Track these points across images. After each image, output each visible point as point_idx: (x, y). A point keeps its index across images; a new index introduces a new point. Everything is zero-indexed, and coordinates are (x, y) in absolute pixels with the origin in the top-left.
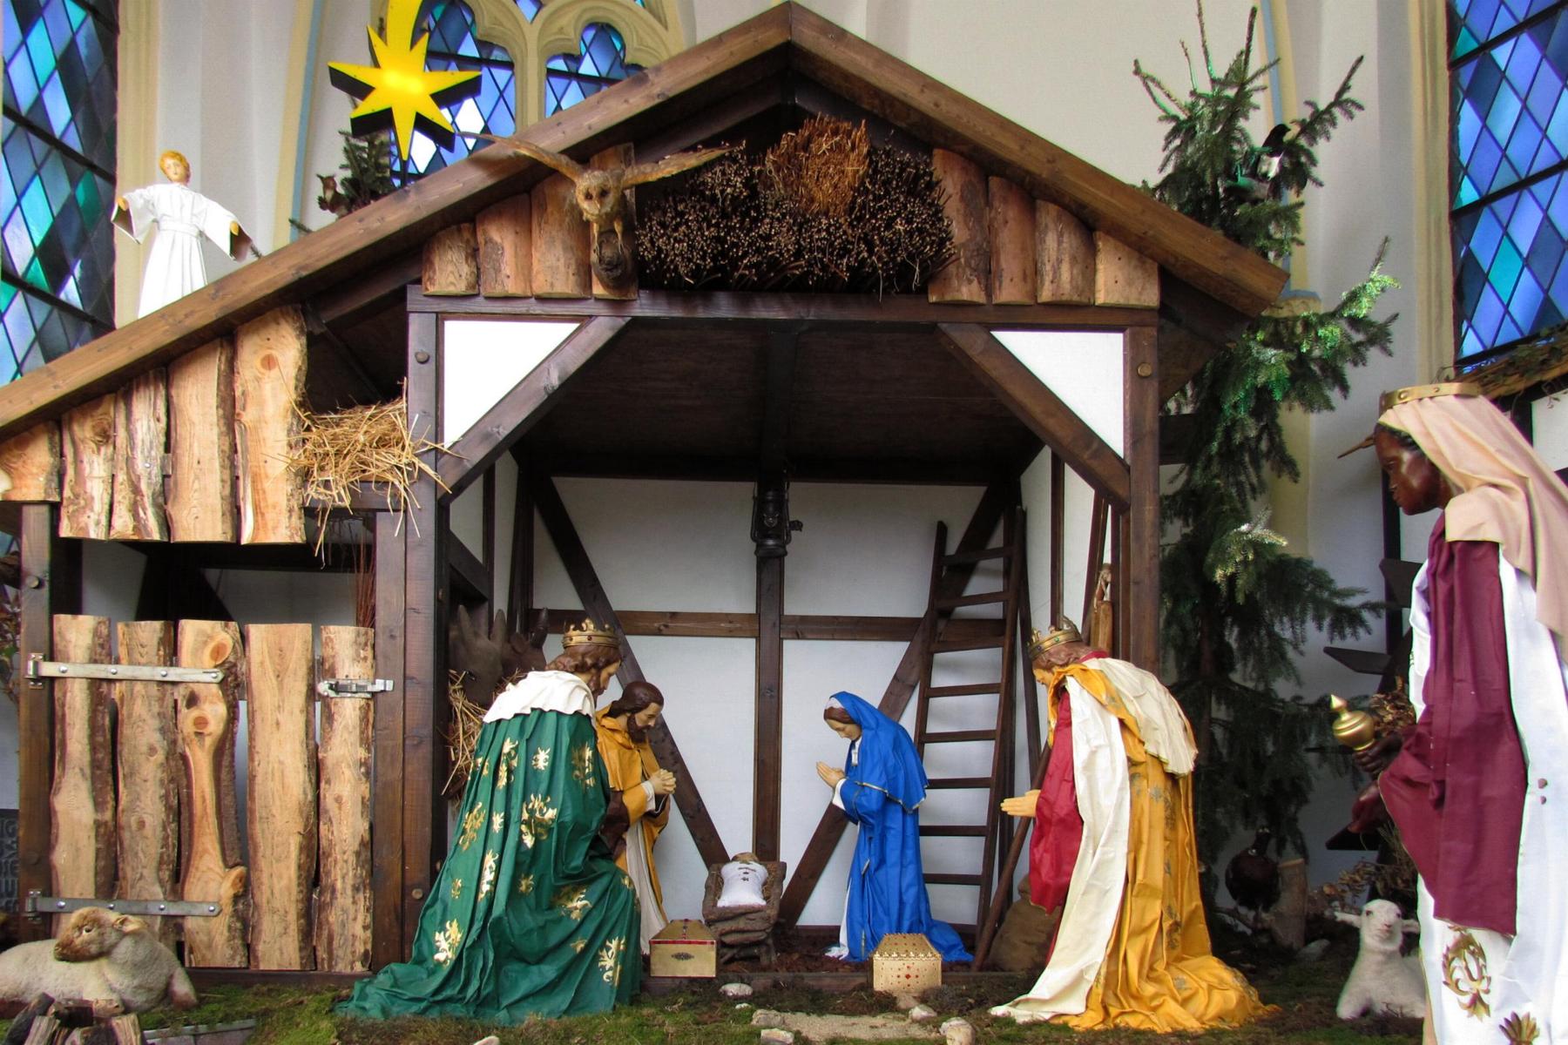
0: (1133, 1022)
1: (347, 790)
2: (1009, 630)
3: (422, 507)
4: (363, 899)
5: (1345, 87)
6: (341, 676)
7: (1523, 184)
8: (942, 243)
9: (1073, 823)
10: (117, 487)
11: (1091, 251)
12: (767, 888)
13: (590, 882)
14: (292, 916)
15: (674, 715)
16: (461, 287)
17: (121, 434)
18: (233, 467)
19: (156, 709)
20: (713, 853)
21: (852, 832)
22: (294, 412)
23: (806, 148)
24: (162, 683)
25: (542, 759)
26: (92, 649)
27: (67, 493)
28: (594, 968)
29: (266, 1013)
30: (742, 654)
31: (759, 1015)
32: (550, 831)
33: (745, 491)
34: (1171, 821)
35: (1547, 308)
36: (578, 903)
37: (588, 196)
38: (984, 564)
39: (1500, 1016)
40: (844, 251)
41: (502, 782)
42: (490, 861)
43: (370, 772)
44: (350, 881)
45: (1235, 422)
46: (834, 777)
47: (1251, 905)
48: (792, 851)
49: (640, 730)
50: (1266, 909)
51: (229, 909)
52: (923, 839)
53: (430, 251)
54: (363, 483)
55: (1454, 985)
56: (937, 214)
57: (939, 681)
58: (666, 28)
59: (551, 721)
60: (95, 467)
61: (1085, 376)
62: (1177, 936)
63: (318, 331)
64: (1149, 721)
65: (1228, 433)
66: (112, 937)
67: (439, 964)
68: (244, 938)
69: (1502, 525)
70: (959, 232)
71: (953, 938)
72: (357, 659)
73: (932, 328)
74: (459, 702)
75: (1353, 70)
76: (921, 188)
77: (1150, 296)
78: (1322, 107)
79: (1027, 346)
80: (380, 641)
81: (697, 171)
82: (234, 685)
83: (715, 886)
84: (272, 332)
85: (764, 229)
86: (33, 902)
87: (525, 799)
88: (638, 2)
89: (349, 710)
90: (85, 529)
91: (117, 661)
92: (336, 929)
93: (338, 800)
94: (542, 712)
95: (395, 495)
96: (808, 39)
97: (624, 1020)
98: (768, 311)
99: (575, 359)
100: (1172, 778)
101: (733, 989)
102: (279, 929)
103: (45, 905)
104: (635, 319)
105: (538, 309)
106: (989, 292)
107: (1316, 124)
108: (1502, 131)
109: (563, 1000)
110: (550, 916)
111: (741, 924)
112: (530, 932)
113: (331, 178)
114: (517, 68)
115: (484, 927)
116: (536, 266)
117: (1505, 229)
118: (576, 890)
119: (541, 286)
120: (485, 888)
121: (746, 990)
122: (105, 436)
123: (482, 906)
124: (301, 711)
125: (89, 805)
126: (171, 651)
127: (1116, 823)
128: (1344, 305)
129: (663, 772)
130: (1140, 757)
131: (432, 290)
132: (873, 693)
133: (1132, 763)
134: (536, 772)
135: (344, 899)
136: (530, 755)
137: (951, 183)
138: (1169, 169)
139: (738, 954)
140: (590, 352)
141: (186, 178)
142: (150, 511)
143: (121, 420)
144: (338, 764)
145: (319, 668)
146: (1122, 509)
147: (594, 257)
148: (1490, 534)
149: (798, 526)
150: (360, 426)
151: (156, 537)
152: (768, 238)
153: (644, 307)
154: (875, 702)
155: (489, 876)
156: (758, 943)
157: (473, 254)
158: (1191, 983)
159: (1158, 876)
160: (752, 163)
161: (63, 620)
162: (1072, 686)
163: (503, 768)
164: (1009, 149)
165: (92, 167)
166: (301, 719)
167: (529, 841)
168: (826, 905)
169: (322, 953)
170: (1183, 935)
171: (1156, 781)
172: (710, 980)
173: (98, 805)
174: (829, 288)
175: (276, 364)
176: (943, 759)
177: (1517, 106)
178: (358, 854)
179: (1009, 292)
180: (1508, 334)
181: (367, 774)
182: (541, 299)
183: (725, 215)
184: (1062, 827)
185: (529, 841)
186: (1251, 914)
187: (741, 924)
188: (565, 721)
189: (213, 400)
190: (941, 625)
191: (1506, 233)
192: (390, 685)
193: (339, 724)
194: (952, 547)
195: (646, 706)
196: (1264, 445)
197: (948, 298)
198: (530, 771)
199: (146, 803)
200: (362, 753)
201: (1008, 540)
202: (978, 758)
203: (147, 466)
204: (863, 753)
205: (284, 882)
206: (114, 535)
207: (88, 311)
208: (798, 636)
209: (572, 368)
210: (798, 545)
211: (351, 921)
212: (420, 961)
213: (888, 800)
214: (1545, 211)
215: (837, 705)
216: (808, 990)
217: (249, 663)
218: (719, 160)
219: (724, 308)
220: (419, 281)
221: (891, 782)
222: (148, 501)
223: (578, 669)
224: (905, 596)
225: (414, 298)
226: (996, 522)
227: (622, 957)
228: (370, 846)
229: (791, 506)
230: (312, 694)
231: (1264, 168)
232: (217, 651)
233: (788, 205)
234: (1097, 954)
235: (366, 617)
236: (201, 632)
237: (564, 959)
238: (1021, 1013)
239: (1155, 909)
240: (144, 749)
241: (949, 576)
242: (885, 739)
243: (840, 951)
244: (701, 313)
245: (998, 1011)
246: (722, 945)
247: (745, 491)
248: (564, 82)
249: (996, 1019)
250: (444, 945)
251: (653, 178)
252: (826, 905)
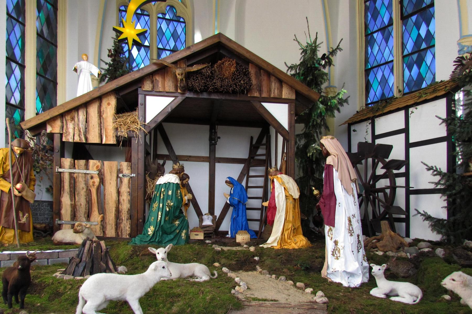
0: (286, 247)
1: (125, 197)
2: (266, 163)
3: (141, 136)
4: (129, 222)
5: (339, 46)
6: (124, 173)
7: (379, 66)
8: (251, 86)
9: (275, 208)
10: (75, 130)
11: (281, 87)
12: (213, 221)
13: (179, 218)
14: (114, 225)
15: (191, 182)
16: (150, 89)
17: (76, 119)
18: (101, 127)
19: (84, 179)
20: (199, 214)
21: (231, 209)
22: (114, 116)
23: (223, 64)
24: (85, 174)
25: (170, 193)
26: (70, 166)
27: (64, 131)
28: (180, 236)
29: (113, 245)
30: (206, 166)
31: (214, 246)
32: (172, 207)
33: (208, 127)
34: (294, 208)
35: (383, 94)
36: (177, 223)
37: (179, 75)
38: (261, 147)
39: (333, 240)
40: (231, 86)
41: (162, 197)
42: (160, 213)
43: (130, 194)
44: (126, 218)
45: (314, 119)
46: (227, 196)
47: (318, 227)
48: (217, 213)
49: (184, 185)
50: (321, 228)
51: (100, 224)
52: (247, 211)
53: (143, 81)
54: (130, 131)
55: (329, 236)
56: (250, 80)
57: (251, 173)
58: (187, 8)
59: (172, 185)
60: (71, 126)
61: (280, 113)
62: (295, 231)
63: (119, 97)
64: (290, 188)
65: (313, 121)
66: (84, 228)
67: (149, 235)
68: (103, 230)
69: (334, 163)
70: (254, 81)
71: (254, 233)
72: (128, 169)
73: (249, 101)
74: (148, 179)
75: (341, 41)
76: (247, 74)
77: (294, 97)
78: (334, 49)
79: (268, 106)
80: (133, 166)
81: (201, 69)
82: (101, 175)
83: (201, 220)
84: (109, 98)
85: (214, 81)
86: (57, 222)
87: (167, 201)
88: (180, 1)
89: (126, 180)
90: (69, 139)
91: (75, 169)
92: (123, 228)
93: (123, 200)
94: (170, 183)
95: (136, 134)
96: (223, 41)
97: (187, 246)
98: (214, 97)
99: (174, 106)
100: (294, 199)
101: (207, 241)
102: (111, 228)
103: (59, 222)
104: (187, 97)
105: (166, 94)
106: (260, 94)
107: (333, 52)
108: (375, 53)
109: (175, 242)
110: (172, 225)
111: (208, 229)
112: (168, 228)
113: (110, 50)
114: (150, 16)
115: (159, 227)
116: (166, 85)
117: (375, 75)
118: (176, 220)
119: (167, 89)
120: (159, 219)
121: (210, 242)
122: (73, 119)
123: (158, 223)
124: (116, 179)
125: (69, 200)
126: (87, 167)
127: (283, 208)
128: (336, 96)
129: (189, 194)
130: (288, 195)
131: (144, 90)
132: (236, 177)
133: (286, 196)
134: (169, 195)
135: (125, 222)
136: (168, 191)
137: (252, 70)
138: (302, 60)
139: (207, 236)
140: (177, 104)
141: (87, 60)
142: (83, 136)
143: (76, 115)
144: (123, 192)
145: (119, 171)
146: (288, 141)
147: (179, 85)
148: (332, 164)
149: (219, 138)
150: (128, 118)
151: (84, 142)
152: (215, 83)
153: (188, 95)
154: (236, 179)
155: (160, 217)
156: (211, 233)
157: (152, 82)
158: (297, 240)
159: (291, 219)
160: (212, 68)
161: (63, 159)
162: (275, 180)
163: (162, 194)
164: (265, 66)
165: (52, 44)
166: (115, 182)
167: (168, 209)
168: (225, 226)
169: (120, 233)
170: (296, 231)
171: (291, 200)
172: (202, 240)
173: (71, 200)
174: (227, 93)
175: (110, 106)
176: (252, 192)
177: (378, 48)
178: (128, 212)
179: (265, 95)
180: (376, 100)
181: (129, 194)
182: (167, 92)
183: (206, 78)
184: (273, 208)
185: (168, 209)
186: (317, 229)
187: (208, 229)
188: (175, 185)
189: (97, 112)
190: (252, 160)
191: (376, 76)
192: (135, 175)
193: (124, 183)
194: (254, 142)
195: (186, 179)
196: (322, 123)
197: (252, 96)
198: (168, 195)
199: (82, 200)
200: (129, 190)
201: (267, 141)
202: (259, 192)
203: (82, 126)
204: (234, 191)
205: (112, 218)
206: (75, 141)
207: (52, 79)
208: (219, 162)
209: (174, 107)
210: (219, 142)
211: (126, 226)
212: (144, 234)
213: (239, 202)
214: (383, 73)
215: (228, 180)
216: (223, 242)
217: (104, 170)
218: (206, 67)
219: (205, 96)
220: (141, 87)
221: (240, 198)
222: (82, 134)
223: (176, 173)
224: (243, 154)
225: (140, 91)
226: (264, 137)
227: (186, 234)
228: (130, 211)
229: (218, 133)
230: (118, 177)
231: (321, 63)
232: (97, 167)
233: (219, 76)
234: (279, 234)
235: (129, 159)
236: (94, 163)
237: (175, 234)
238: (265, 246)
239: (290, 225)
240: (81, 188)
241: (253, 149)
242: (239, 188)
243: (229, 236)
244: (201, 97)
245: (261, 246)
246: (204, 234)
247: (208, 127)
248: (162, 20)
249: (260, 247)
250: (150, 231)
251: (192, 71)
252: (225, 226)
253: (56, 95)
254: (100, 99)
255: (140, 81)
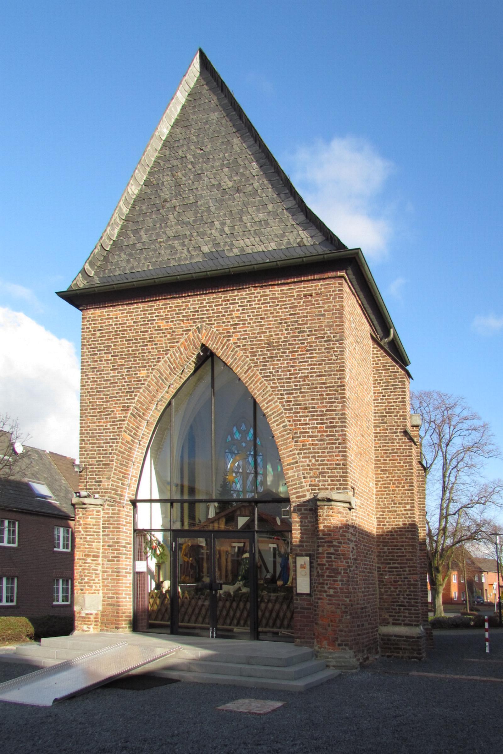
1: (230, 564)
253: (254, 127)
254: (219, 519)
255: (234, 511)
